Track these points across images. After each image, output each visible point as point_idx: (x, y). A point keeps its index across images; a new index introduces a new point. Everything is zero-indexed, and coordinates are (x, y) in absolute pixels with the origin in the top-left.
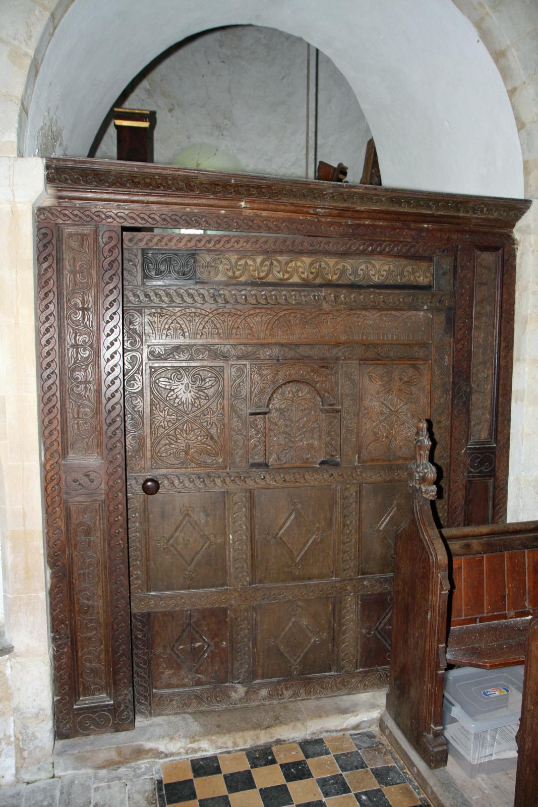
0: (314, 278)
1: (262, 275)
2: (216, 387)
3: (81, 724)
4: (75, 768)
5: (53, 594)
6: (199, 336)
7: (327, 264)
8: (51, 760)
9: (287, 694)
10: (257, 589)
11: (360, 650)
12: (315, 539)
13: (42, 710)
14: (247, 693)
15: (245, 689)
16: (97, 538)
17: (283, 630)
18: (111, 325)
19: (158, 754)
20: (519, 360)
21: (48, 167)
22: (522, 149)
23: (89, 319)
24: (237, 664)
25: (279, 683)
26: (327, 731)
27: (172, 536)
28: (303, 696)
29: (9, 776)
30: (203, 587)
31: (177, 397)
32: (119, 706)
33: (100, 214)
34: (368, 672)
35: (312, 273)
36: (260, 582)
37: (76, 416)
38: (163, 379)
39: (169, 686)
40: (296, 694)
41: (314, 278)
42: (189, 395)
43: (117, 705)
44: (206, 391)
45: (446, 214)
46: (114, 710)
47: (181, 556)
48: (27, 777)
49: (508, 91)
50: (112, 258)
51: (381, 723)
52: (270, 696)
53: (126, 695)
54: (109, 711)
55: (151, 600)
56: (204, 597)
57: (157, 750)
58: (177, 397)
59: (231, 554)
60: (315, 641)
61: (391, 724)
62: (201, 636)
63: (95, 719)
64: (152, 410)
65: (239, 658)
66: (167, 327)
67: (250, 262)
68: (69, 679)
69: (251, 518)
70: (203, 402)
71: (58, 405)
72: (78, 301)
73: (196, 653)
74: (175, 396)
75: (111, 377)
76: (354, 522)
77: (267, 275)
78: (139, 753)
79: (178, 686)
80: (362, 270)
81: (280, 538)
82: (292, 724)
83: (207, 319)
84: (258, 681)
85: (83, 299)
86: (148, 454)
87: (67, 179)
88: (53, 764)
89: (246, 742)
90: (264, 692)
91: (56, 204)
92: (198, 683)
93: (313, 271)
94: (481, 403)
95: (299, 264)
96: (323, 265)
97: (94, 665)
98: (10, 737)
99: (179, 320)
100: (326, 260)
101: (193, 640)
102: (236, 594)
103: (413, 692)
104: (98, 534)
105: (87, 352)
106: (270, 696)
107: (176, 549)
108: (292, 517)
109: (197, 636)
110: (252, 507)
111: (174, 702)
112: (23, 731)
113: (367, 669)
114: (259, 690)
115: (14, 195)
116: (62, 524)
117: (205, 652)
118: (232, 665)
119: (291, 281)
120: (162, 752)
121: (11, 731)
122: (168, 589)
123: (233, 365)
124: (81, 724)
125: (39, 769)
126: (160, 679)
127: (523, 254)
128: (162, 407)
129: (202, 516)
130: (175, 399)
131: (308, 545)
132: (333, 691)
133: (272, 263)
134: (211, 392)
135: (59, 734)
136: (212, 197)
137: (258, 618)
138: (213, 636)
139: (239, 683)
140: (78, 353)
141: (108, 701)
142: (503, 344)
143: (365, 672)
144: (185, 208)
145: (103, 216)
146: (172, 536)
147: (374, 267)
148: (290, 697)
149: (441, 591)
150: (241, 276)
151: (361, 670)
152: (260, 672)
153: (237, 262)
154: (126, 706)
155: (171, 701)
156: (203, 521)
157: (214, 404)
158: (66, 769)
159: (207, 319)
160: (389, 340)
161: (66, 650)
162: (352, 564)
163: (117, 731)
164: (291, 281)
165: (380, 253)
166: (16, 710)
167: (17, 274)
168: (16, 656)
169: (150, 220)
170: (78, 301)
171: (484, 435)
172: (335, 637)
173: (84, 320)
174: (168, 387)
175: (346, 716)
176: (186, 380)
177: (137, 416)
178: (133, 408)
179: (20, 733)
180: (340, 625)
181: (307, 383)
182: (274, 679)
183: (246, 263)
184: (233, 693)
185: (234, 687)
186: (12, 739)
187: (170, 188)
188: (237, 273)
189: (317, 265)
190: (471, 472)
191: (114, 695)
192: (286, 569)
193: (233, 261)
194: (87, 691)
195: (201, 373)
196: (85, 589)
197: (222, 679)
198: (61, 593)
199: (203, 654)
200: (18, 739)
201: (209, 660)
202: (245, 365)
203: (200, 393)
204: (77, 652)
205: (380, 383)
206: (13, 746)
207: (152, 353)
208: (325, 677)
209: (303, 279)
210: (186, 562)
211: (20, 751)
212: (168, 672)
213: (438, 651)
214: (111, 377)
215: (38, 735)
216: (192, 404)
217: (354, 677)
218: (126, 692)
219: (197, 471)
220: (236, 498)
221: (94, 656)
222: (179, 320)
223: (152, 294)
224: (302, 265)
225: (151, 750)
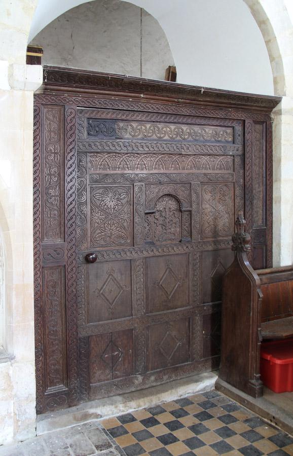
2: (126, 199)
4: (48, 430)
6: (117, 169)
7: (182, 129)
8: (35, 426)
9: (165, 377)
12: (179, 284)
13: (31, 395)
14: (143, 379)
17: (162, 340)
18: (71, 162)
19: (97, 416)
20: (276, 181)
21: (44, 71)
22: (273, 71)
23: (57, 159)
24: (138, 363)
25: (161, 372)
27: (102, 288)
28: (174, 378)
29: (9, 439)
30: (119, 318)
31: (105, 205)
33: (66, 99)
34: (207, 360)
36: (151, 312)
37: (49, 216)
38: (98, 194)
39: (99, 381)
42: (112, 204)
43: (70, 390)
44: (121, 201)
46: (68, 394)
47: (107, 300)
48: (20, 438)
49: (265, 42)
50: (72, 124)
52: (156, 380)
54: (65, 394)
55: (87, 329)
56: (123, 323)
57: (96, 413)
58: (105, 205)
60: (179, 344)
61: (225, 384)
62: (118, 347)
64: (91, 213)
65: (139, 359)
66: (100, 163)
67: (143, 128)
68: (44, 376)
69: (146, 275)
70: (120, 207)
71: (40, 209)
72: (52, 148)
74: (104, 204)
75: (70, 192)
76: (199, 273)
78: (86, 416)
81: (161, 285)
82: (170, 391)
83: (122, 159)
84: (149, 372)
85: (55, 147)
86: (89, 240)
88: (36, 428)
89: (145, 404)
90: (153, 378)
91: (42, 93)
94: (258, 204)
98: (11, 413)
99: (106, 159)
101: (113, 351)
102: (137, 320)
103: (241, 361)
105: (56, 178)
106: (156, 380)
107: (104, 296)
108: (167, 273)
110: (147, 268)
111: (103, 391)
112: (19, 409)
114: (150, 377)
115: (25, 86)
118: (135, 364)
119: (164, 138)
120: (99, 415)
125: (28, 432)
126: (94, 377)
127: (276, 125)
128: (97, 211)
129: (119, 275)
130: (104, 206)
131: (175, 288)
132: (189, 374)
134: (124, 201)
135: (39, 412)
136: (127, 91)
139: (139, 374)
140: (51, 178)
141: (64, 388)
142: (268, 173)
143: (206, 360)
145: (67, 101)
146: (102, 288)
148: (167, 379)
149: (258, 298)
150: (139, 135)
152: (150, 366)
153: (136, 127)
154: (75, 391)
156: (119, 278)
157: (126, 209)
158: (44, 431)
159: (122, 159)
161: (41, 359)
162: (198, 297)
163: (70, 406)
164: (164, 138)
169: (92, 103)
170: (52, 148)
171: (260, 222)
173: (55, 159)
174: (100, 199)
176: (110, 195)
177: (83, 217)
178: (81, 212)
179: (17, 410)
180: (193, 334)
182: (158, 370)
185: (136, 377)
186: (12, 415)
187: (107, 86)
188: (136, 134)
190: (255, 242)
191: (67, 385)
192: (164, 304)
193: (148, 127)
195: (119, 190)
200: (16, 414)
201: (122, 362)
202: (142, 185)
203: (118, 202)
204: (46, 360)
205: (210, 195)
206: (12, 419)
207: (92, 178)
210: (110, 303)
212: (99, 373)
213: (257, 332)
214: (70, 192)
216: (114, 209)
219: (117, 248)
220: (137, 263)
221: (57, 358)
222: (106, 159)
223: (92, 144)
224: (176, 139)
225: (93, 414)
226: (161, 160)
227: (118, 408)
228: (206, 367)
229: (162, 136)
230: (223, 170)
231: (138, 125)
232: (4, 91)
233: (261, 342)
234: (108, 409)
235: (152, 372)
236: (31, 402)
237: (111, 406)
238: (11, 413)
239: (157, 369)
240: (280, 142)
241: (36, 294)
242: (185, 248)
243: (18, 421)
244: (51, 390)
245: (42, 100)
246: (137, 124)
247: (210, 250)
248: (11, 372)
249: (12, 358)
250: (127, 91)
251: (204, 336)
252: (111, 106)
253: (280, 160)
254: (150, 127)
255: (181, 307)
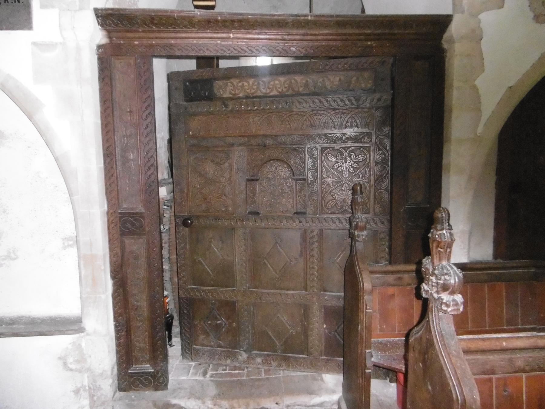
0: (288, 91)
1: (253, 91)
3: (133, 383)
5: (115, 296)
7: (296, 81)
9: (274, 364)
10: (252, 292)
11: (324, 344)
14: (248, 357)
15: (247, 355)
16: (143, 261)
26: (298, 405)
32: (158, 373)
35: (285, 88)
39: (203, 345)
40: (279, 366)
41: (288, 91)
45: (383, 32)
51: (339, 403)
53: (162, 366)
54: (151, 376)
59: (237, 268)
63: (142, 381)
67: (246, 84)
73: (218, 328)
77: (256, 91)
79: (207, 346)
80: (320, 82)
87: (110, 24)
92: (220, 347)
93: (286, 86)
95: (277, 82)
96: (293, 81)
97: (142, 345)
100: (296, 78)
104: (143, 259)
109: (218, 317)
113: (329, 358)
116: (118, 251)
117: (223, 328)
121: (86, 383)
122: (201, 285)
123: (326, 148)
124: (133, 383)
133: (258, 83)
137: (255, 311)
138: (228, 318)
143: (327, 360)
144: (193, 41)
147: (329, 80)
151: (324, 357)
155: (204, 354)
160: (366, 309)
161: (123, 333)
163: (156, 390)
165: (332, 70)
166: (89, 370)
167: (81, 88)
168: (88, 334)
172: (306, 331)
175: (313, 396)
181: (277, 160)
182: (266, 353)
183: (243, 84)
184: (240, 357)
186: (87, 388)
189: (288, 82)
191: (154, 365)
193: (251, 83)
194: (137, 362)
196: (135, 295)
197: (235, 345)
198: (119, 296)
199: (222, 329)
204: (131, 335)
206: (88, 393)
208: (299, 358)
209: (279, 92)
211: (92, 396)
215: (103, 387)
217: (319, 361)
218: (162, 364)
226: (288, 119)
227: (206, 404)
228: (327, 369)
229: (237, 92)
230: (356, 128)
231: (240, 82)
232: (56, 44)
233: (385, 352)
234: (194, 403)
235: (258, 352)
236: (105, 378)
237: (198, 401)
238: (85, 386)
239: (264, 351)
240: (451, 85)
241: (112, 264)
242: (297, 222)
243: (94, 396)
244: (135, 368)
245: (107, 58)
246: (237, 81)
247: (164, 267)
248: (83, 344)
249: (81, 330)
250: (209, 31)
251: (327, 331)
252: (195, 52)
253: (451, 111)
254: (253, 84)
255: (293, 290)
